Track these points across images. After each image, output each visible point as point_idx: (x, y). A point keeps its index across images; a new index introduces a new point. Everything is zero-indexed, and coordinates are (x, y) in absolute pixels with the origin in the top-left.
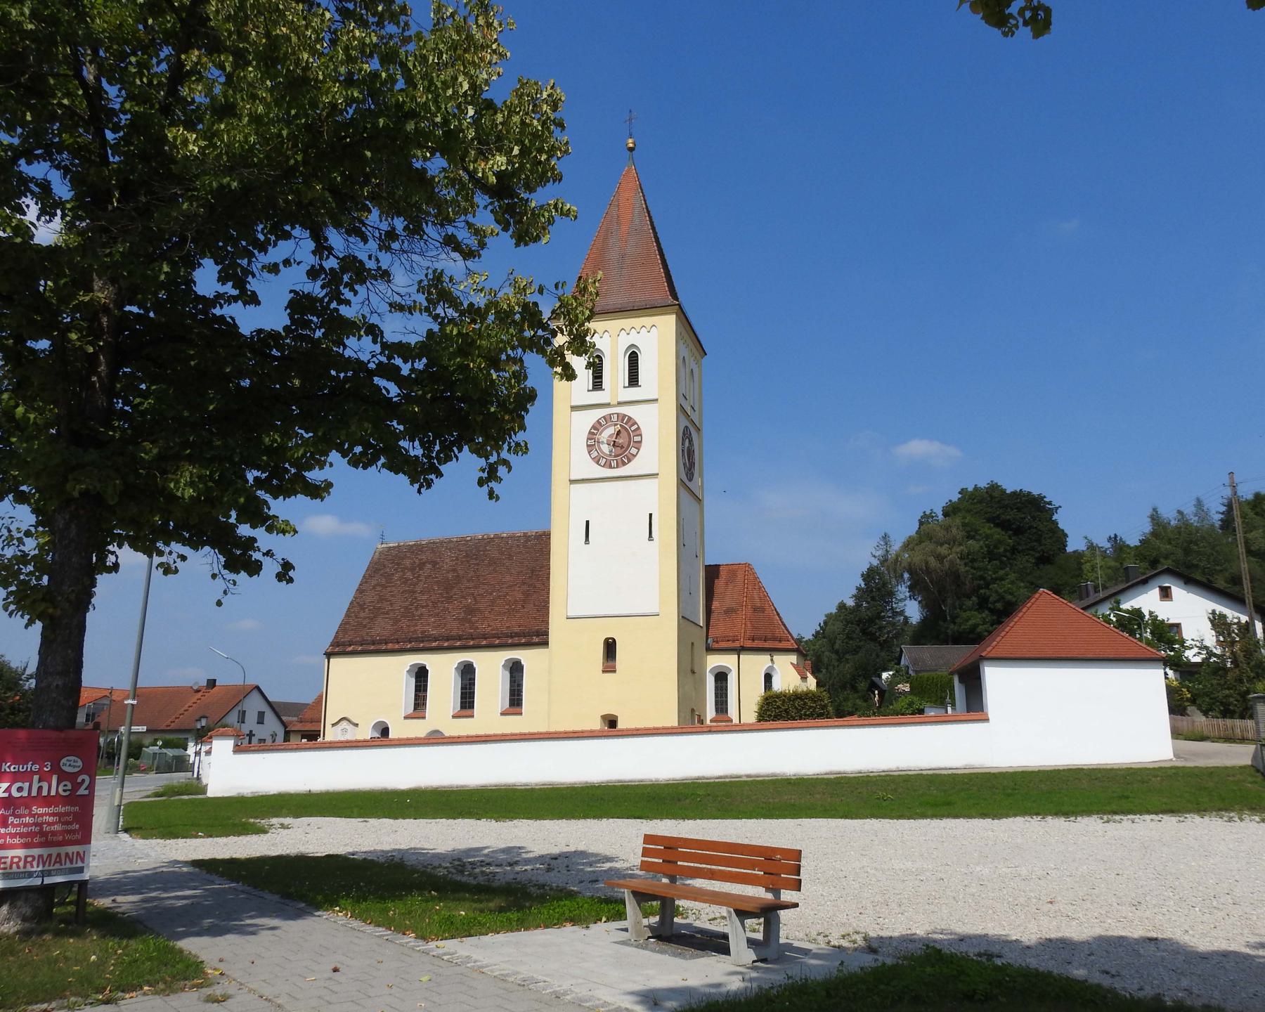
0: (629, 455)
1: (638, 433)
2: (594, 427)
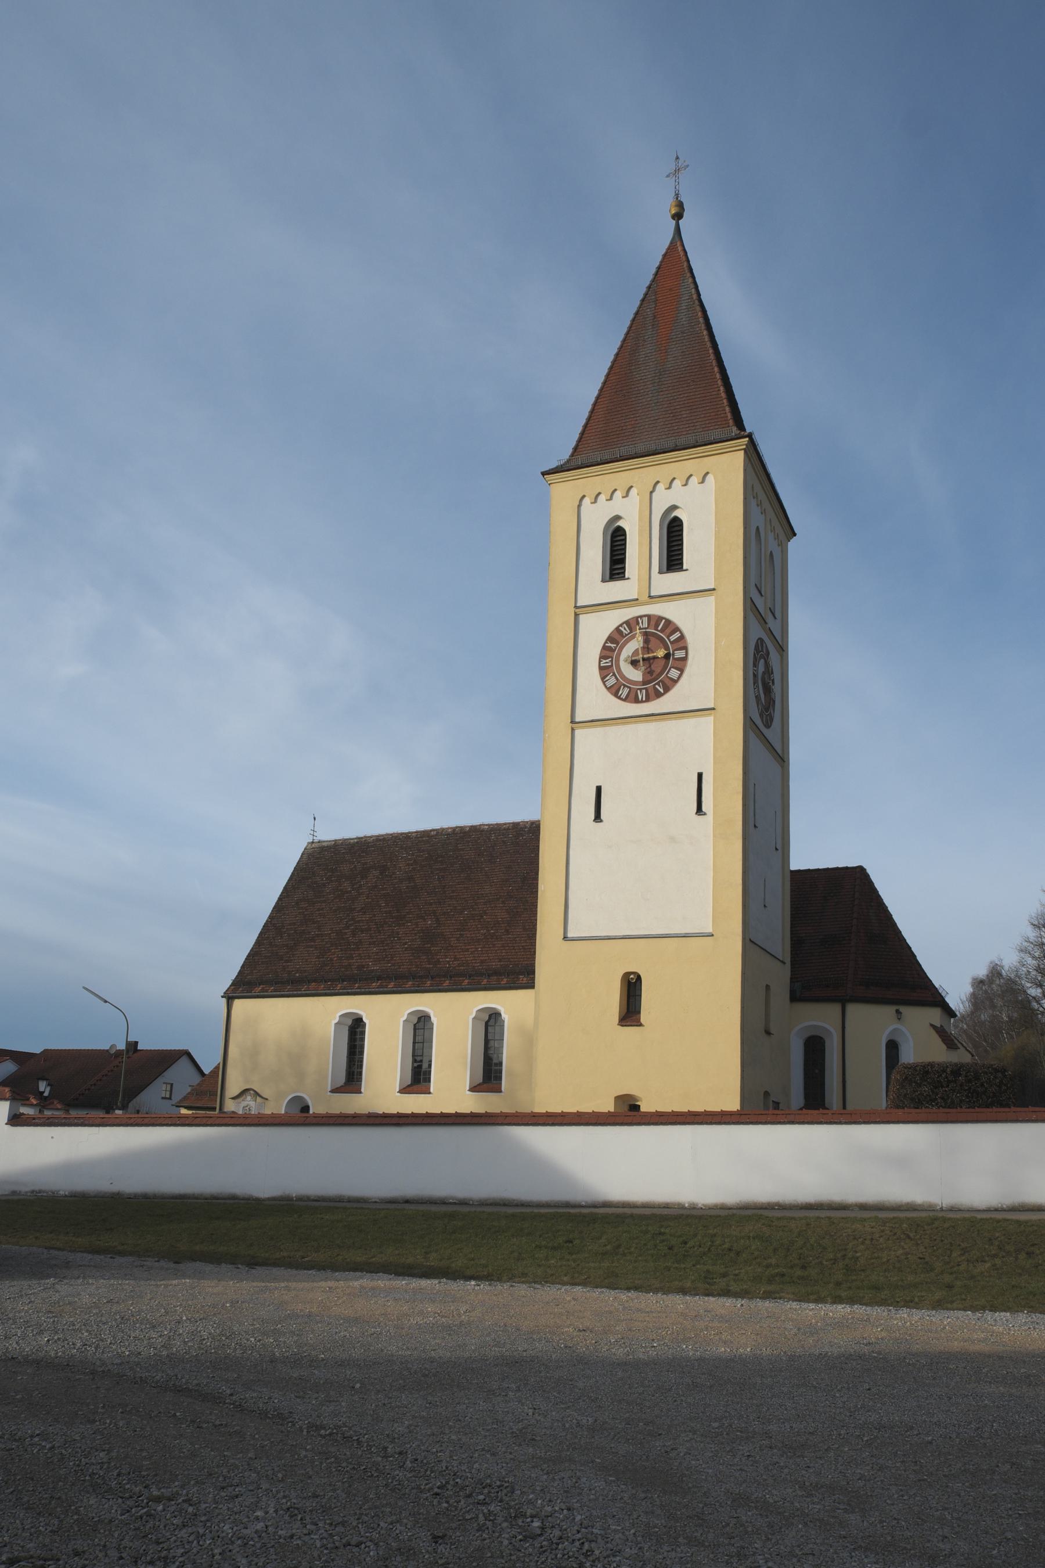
0: (667, 681)
1: (681, 644)
2: (610, 639)
